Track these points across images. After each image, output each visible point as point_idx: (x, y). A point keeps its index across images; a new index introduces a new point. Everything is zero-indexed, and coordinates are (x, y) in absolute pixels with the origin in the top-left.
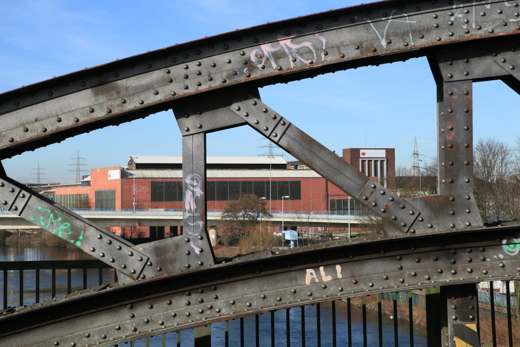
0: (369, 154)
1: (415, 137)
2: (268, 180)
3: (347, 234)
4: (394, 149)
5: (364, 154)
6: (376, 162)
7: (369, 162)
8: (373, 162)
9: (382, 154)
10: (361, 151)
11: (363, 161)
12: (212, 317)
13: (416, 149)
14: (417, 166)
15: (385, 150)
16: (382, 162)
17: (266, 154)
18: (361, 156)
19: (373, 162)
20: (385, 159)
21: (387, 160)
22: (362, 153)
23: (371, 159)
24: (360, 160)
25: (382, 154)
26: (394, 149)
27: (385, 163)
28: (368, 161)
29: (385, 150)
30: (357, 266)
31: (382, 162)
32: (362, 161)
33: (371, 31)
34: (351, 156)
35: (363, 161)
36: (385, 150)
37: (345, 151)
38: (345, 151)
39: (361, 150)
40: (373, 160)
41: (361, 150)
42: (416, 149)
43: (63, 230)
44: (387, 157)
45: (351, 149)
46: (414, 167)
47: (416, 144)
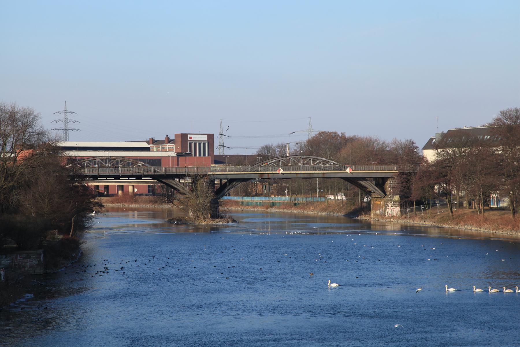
0: (195, 138)
1: (221, 120)
4: (213, 134)
5: (191, 138)
6: (200, 144)
7: (195, 144)
8: (198, 144)
9: (204, 138)
10: (189, 136)
11: (191, 144)
13: (221, 130)
14: (223, 145)
15: (206, 136)
16: (204, 144)
17: (60, 129)
18: (189, 139)
20: (207, 142)
22: (190, 137)
23: (196, 142)
24: (189, 142)
25: (204, 138)
28: (199, 143)
29: (206, 135)
30: (496, 117)
31: (204, 144)
32: (190, 143)
33: (358, 197)
35: (191, 144)
36: (206, 135)
37: (176, 135)
38: (176, 135)
39: (189, 135)
40: (202, 142)
41: (189, 135)
42: (221, 130)
44: (208, 140)
45: (182, 134)
47: (221, 126)
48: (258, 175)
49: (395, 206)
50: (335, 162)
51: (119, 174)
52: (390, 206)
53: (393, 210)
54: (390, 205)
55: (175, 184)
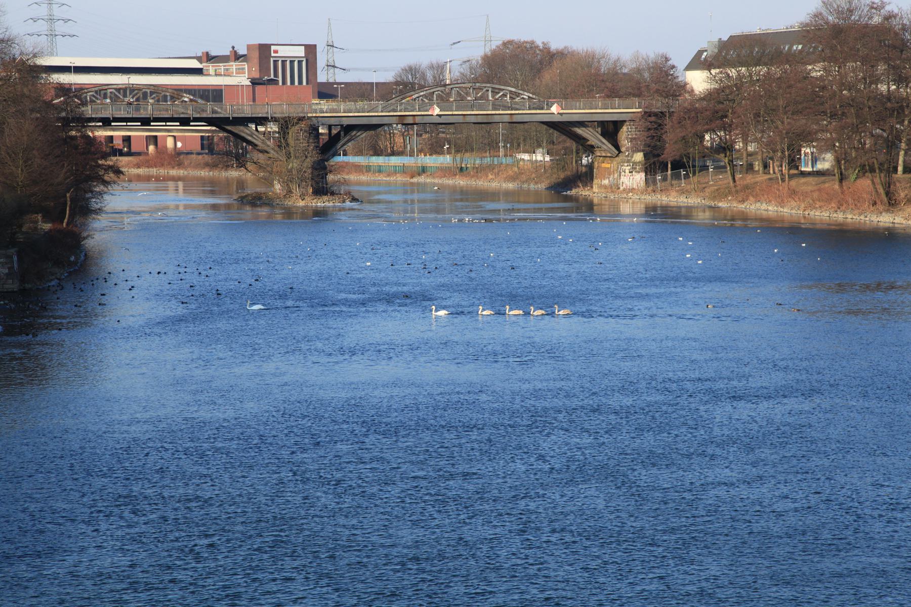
0: (284, 52)
2: (219, 88)
3: (421, 205)
4: (315, 46)
5: (276, 52)
6: (292, 62)
7: (284, 62)
9: (300, 52)
10: (273, 48)
11: (275, 62)
12: (397, 284)
13: (330, 37)
16: (300, 62)
18: (273, 54)
19: (288, 63)
20: (304, 60)
21: (307, 61)
24: (272, 60)
25: (300, 52)
26: (315, 46)
27: (304, 64)
31: (300, 62)
34: (260, 54)
35: (275, 62)
37: (249, 47)
38: (249, 47)
42: (330, 37)
43: (746, 143)
44: (306, 56)
46: (328, 66)
48: (395, 118)
49: (636, 172)
50: (531, 95)
51: (148, 116)
52: (627, 171)
53: (631, 178)
54: (627, 169)
55: (249, 135)
